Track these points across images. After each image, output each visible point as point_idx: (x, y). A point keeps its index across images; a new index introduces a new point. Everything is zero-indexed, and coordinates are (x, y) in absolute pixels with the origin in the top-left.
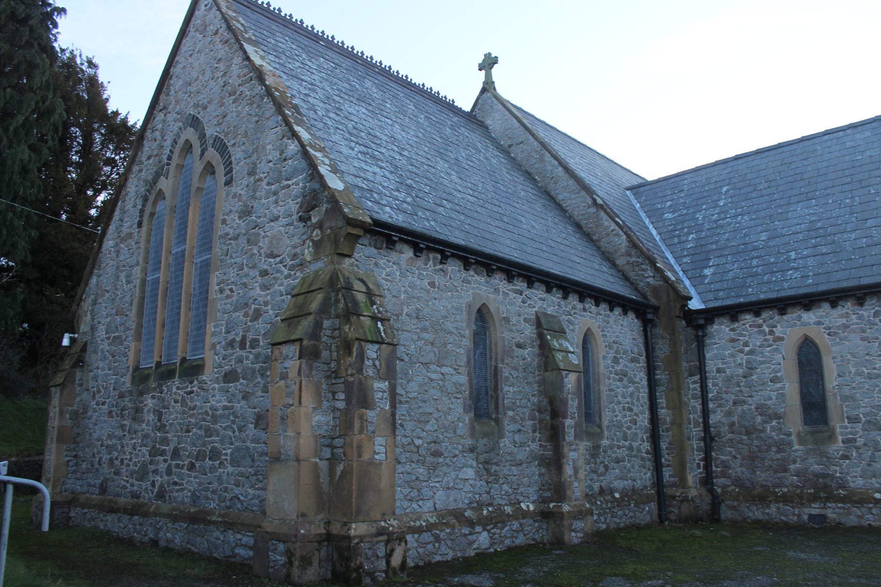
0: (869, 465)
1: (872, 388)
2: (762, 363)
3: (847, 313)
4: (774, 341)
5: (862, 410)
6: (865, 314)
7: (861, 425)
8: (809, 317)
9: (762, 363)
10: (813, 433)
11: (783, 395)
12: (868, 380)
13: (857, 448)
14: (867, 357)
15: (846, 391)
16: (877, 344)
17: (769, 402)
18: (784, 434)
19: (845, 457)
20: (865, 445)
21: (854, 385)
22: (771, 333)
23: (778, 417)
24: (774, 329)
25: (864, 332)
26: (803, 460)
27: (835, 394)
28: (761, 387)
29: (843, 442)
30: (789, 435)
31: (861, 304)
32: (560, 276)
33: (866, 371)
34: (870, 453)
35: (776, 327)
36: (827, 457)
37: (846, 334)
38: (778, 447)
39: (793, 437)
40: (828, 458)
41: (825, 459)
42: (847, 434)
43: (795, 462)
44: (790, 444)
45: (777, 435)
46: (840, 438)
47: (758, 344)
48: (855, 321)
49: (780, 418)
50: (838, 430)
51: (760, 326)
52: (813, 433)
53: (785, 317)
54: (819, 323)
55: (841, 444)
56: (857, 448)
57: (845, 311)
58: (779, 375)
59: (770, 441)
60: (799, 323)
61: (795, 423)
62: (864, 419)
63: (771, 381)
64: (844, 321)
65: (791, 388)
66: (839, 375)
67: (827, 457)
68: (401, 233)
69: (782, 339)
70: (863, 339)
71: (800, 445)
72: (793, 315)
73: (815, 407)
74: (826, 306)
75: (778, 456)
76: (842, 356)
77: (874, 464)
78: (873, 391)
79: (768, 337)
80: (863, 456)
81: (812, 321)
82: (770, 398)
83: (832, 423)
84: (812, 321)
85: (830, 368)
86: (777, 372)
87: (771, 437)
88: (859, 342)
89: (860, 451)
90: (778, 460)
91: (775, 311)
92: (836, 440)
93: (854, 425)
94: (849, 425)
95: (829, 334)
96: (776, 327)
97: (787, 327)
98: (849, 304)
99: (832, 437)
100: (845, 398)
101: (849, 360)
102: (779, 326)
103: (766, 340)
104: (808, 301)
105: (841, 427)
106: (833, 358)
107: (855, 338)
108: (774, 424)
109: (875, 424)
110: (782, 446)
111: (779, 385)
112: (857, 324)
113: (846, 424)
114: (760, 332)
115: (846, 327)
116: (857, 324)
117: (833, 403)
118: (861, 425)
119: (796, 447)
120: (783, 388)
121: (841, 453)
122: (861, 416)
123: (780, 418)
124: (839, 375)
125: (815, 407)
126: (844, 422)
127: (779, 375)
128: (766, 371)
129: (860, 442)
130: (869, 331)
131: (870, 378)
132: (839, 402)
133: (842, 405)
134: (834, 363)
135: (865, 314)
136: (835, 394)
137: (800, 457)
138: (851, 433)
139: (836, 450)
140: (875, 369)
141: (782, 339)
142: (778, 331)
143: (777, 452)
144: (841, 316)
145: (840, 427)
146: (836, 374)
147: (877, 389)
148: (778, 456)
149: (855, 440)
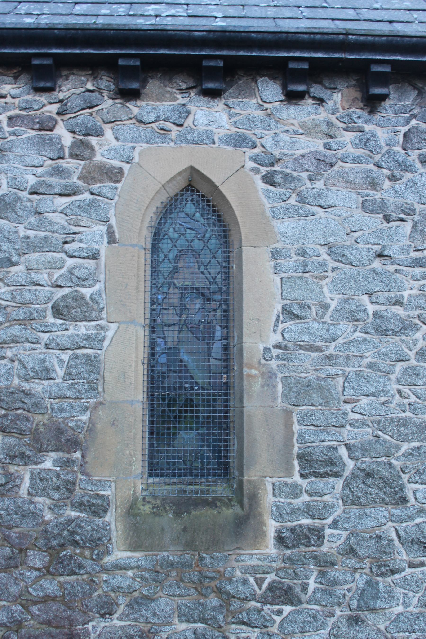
0: (355, 620)
1: (384, 365)
2: (31, 246)
3: (329, 124)
4: (87, 177)
5: (347, 433)
6: (382, 135)
7: (339, 483)
8: (210, 116)
9: (31, 246)
10: (182, 505)
11: (91, 362)
12: (376, 338)
13: (325, 564)
14: (377, 264)
15: (306, 364)
16: (407, 228)
17: (38, 387)
18: (80, 506)
19: (282, 594)
20: (351, 551)
21: (331, 349)
22: (81, 151)
23: (66, 440)
24: (93, 140)
25: (374, 185)
26: (138, 603)
27: (270, 375)
28: (16, 330)
29: (280, 540)
30: (97, 508)
31: (372, 103)
32: (83, 29)
33: (371, 309)
34: (360, 580)
35: (99, 133)
36: (219, 591)
37: (319, 185)
38: (53, 552)
39: (109, 517)
40: (227, 598)
41: (213, 601)
42: (294, 512)
43: (107, 610)
44: (98, 544)
45: (55, 507)
46: (271, 526)
47: (32, 180)
48: (350, 149)
49: (74, 444)
50: (268, 500)
51: (46, 126)
52: (182, 505)
53: (134, 108)
54: (239, 141)
55: (271, 548)
56: (325, 564)
57: (323, 115)
58: (87, 292)
59: (26, 527)
60: (175, 132)
61: (121, 467)
62: (350, 464)
63: (57, 312)
64: (317, 144)
65: (124, 352)
66: (288, 313)
67: (219, 591)
68: (229, 47)
69: (114, 175)
70: (368, 207)
71: (134, 547)
72: (161, 102)
73: (195, 417)
74: (270, 90)
75: (50, 586)
76: (302, 253)
77: (370, 617)
78: (388, 373)
79: (69, 163)
80: (340, 590)
81: (219, 133)
82: (46, 373)
83: (251, 475)
84: (219, 133)
85: (262, 290)
86: (82, 281)
87: (34, 515)
88: (360, 216)
89: (332, 574)
90: (47, 599)
91: (106, 82)
92: (260, 534)
93: (320, 484)
94: (304, 483)
95: (269, 179)
96: (99, 133)
97: (136, 139)
98: (337, 97)
99: (244, 525)
100: (301, 391)
101: (323, 265)
102: (109, 133)
103: (59, 172)
104: (217, 62)
105: (277, 491)
106: (275, 254)
107: (344, 198)
108: (48, 464)
109: (386, 482)
110: (68, 549)
111: (83, 328)
112: (357, 160)
113: (297, 478)
114: (41, 144)
115: (323, 163)
116: (357, 160)
117: (260, 406)
118: (339, 483)
119: (119, 554)
120: (95, 340)
121: (270, 578)
122: (343, 452)
123: (74, 444)
124: (288, 313)
125: (195, 417)
126: (289, 473)
127: (87, 292)
128: (43, 277)
129: (334, 541)
130: (387, 184)
131: (384, 332)
132: (280, 403)
133: (288, 414)
134: (277, 270)
135: (382, 135)
136: (270, 375)
137: (130, 590)
138: (308, 510)
139: (254, 570)
140: (399, 303)
141: (114, 175)
142: (106, 148)
143: (47, 571)
144: (308, 130)
145: (274, 487)
146: (278, 308)
147: (399, 367)
148: (50, 586)
149: (318, 534)
